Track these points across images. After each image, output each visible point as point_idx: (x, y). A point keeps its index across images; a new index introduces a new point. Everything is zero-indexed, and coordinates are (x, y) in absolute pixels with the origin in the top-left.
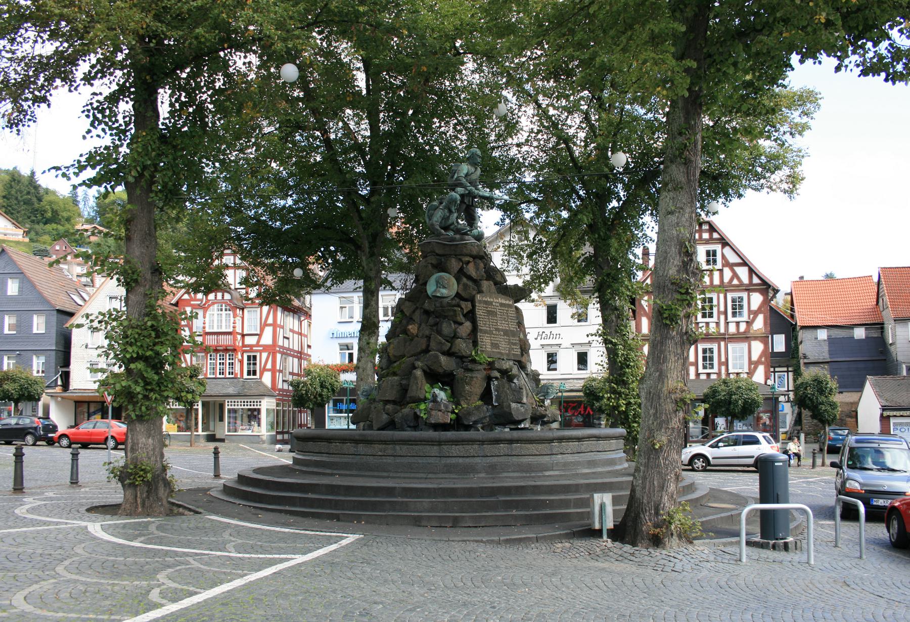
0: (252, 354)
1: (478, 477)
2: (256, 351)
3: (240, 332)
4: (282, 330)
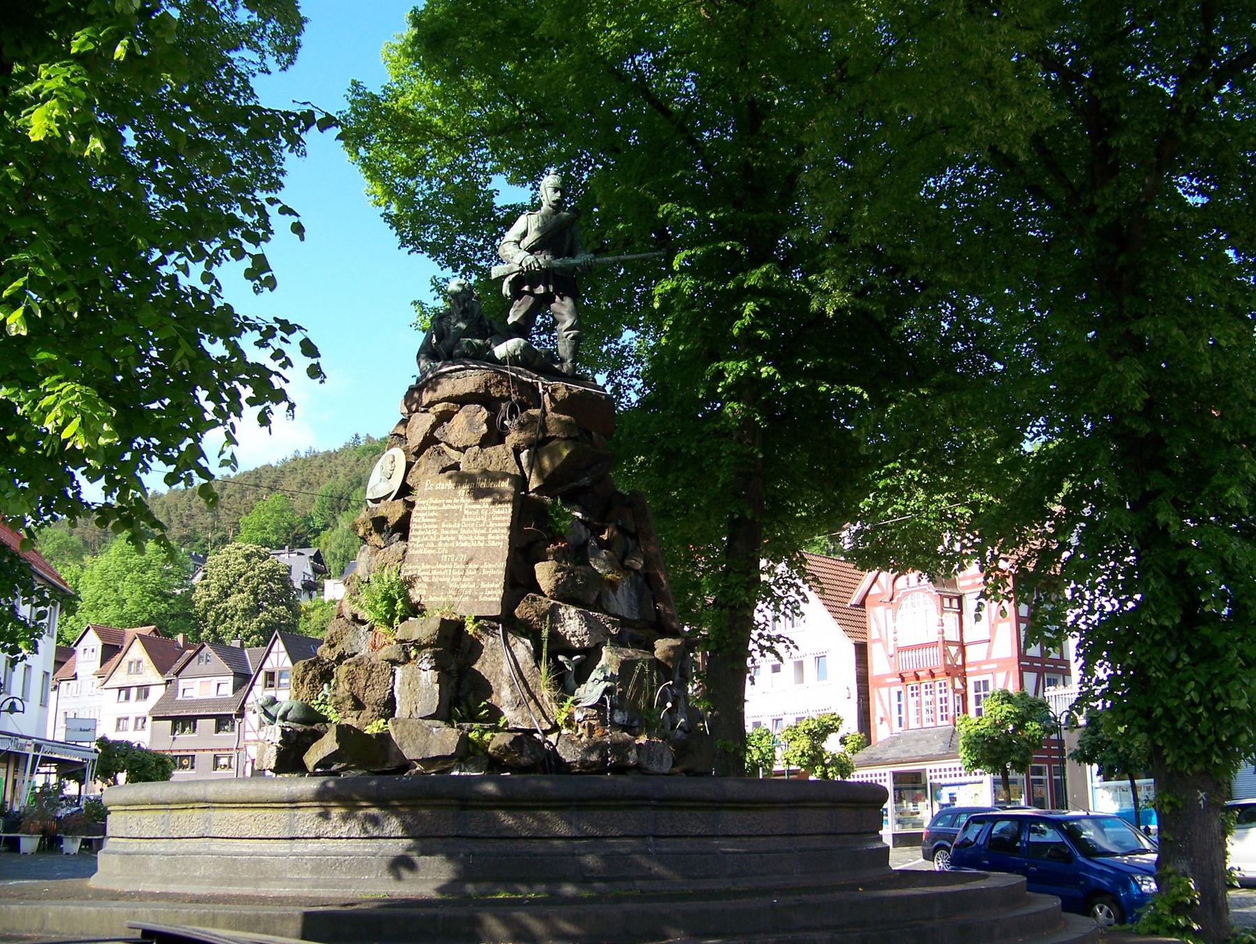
0: (981, 678)
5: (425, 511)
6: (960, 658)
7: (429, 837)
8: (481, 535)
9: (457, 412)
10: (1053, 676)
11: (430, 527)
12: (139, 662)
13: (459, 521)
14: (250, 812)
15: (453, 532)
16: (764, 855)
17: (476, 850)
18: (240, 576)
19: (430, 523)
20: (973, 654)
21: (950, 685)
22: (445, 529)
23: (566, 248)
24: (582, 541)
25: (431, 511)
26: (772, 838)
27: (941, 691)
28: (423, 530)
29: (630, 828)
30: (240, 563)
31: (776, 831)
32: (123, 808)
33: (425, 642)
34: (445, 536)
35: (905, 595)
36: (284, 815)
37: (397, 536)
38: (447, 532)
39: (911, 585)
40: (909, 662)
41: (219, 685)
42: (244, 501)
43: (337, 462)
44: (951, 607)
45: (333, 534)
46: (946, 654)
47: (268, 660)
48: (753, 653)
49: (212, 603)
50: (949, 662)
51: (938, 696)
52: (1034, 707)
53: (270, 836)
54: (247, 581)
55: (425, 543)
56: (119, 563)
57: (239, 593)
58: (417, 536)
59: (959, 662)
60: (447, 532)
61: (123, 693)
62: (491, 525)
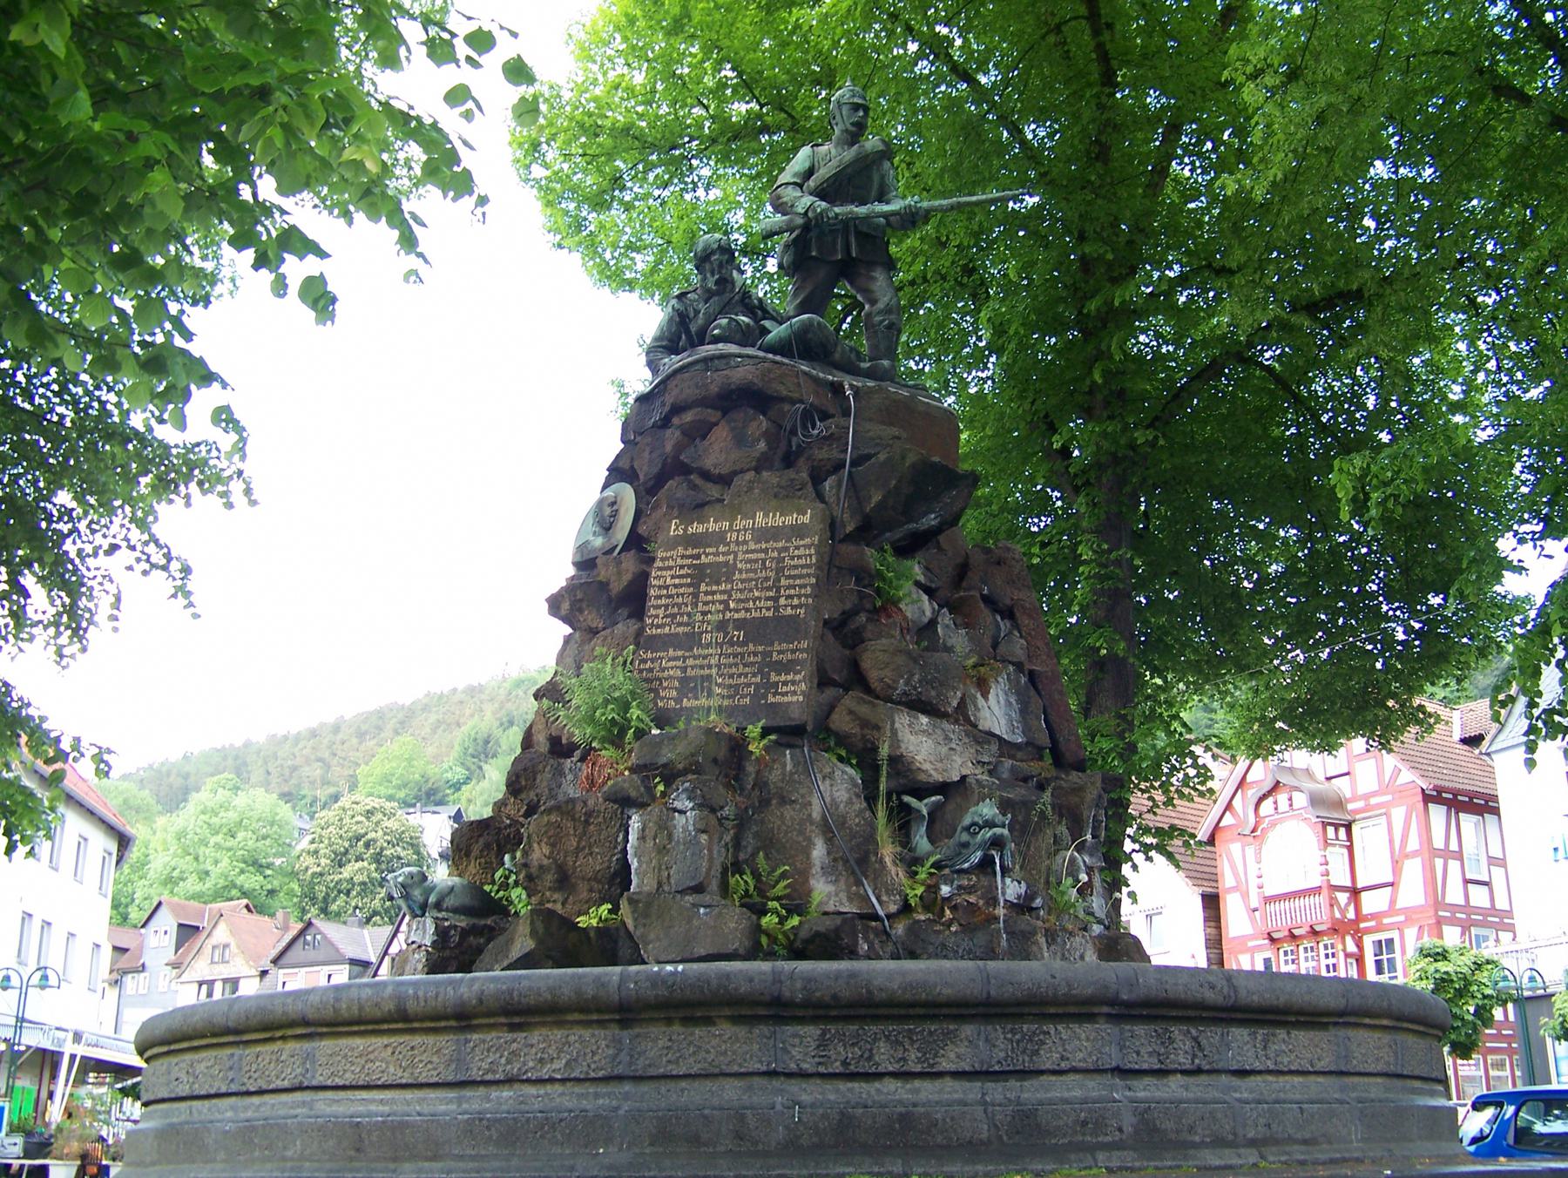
0: (1383, 936)
1: (1157, 1168)
2: (1389, 928)
3: (1349, 884)
4: (1454, 865)
5: (670, 568)
6: (1351, 908)
7: (716, 1076)
8: (767, 599)
9: (716, 424)
10: (1482, 931)
11: (681, 591)
12: (226, 946)
13: (729, 580)
14: (385, 1040)
15: (718, 597)
16: (1305, 1106)
17: (805, 1098)
18: (358, 840)
19: (681, 586)
20: (1372, 902)
21: (1340, 947)
22: (706, 593)
23: (874, 193)
24: (926, 620)
25: (682, 567)
26: (1312, 1078)
27: (1327, 956)
28: (669, 596)
29: (1080, 1055)
30: (358, 823)
31: (1319, 1066)
32: (165, 1049)
33: (680, 766)
34: (706, 603)
35: (1273, 824)
36: (445, 1043)
37: (624, 612)
38: (710, 598)
39: (1280, 810)
40: (1283, 917)
41: (330, 976)
42: (362, 748)
43: (483, 697)
44: (1337, 839)
45: (478, 788)
46: (1333, 903)
47: (395, 940)
48: (1134, 855)
49: (321, 874)
50: (1338, 915)
51: (1324, 962)
52: (1480, 965)
53: (422, 1080)
54: (367, 845)
55: (673, 616)
56: (201, 824)
57: (356, 861)
58: (659, 607)
59: (1351, 915)
60: (710, 598)
61: (204, 987)
62: (783, 582)
